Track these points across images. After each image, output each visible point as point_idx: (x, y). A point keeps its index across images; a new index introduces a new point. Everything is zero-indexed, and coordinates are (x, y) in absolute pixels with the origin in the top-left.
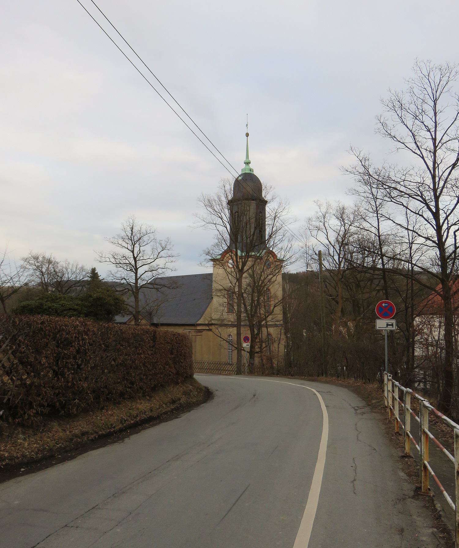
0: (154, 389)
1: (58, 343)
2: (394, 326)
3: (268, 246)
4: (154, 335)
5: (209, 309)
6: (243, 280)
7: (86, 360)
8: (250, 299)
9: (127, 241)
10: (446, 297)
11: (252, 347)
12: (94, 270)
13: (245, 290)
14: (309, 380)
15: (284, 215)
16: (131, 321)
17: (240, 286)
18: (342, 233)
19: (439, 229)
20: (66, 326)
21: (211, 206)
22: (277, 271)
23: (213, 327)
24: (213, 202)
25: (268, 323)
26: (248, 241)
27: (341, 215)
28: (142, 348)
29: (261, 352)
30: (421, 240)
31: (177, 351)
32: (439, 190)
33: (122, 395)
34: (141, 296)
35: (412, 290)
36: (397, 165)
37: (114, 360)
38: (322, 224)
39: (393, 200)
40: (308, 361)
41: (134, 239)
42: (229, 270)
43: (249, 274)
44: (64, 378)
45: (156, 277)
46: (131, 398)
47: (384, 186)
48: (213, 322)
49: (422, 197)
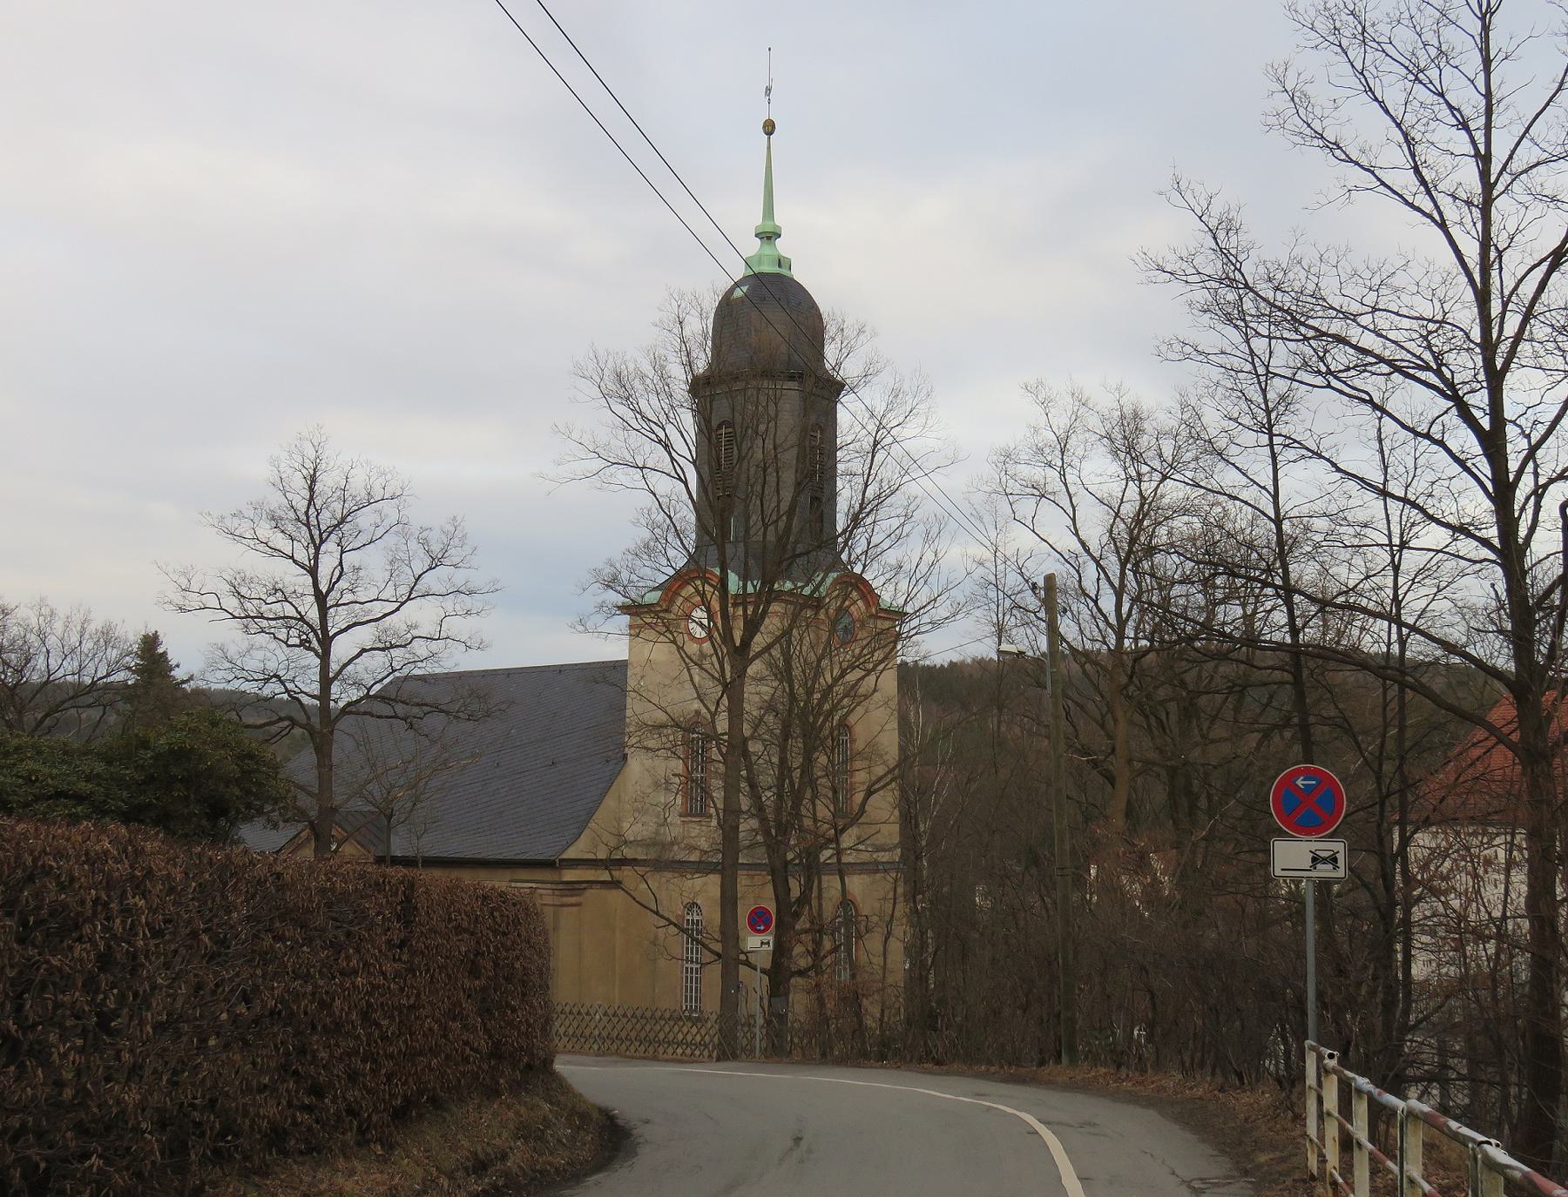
0: (401, 1115)
1: (25, 924)
2: (1341, 863)
3: (844, 557)
4: (408, 900)
5: (610, 802)
6: (749, 689)
7: (136, 995)
8: (775, 760)
9: (290, 528)
10: (1534, 753)
11: (781, 950)
12: (150, 643)
13: (755, 728)
14: (1007, 1080)
15: (915, 438)
16: (300, 847)
17: (736, 713)
18: (1129, 510)
19: (1502, 492)
20: (59, 854)
21: (627, 399)
22: (878, 655)
23: (626, 874)
24: (637, 383)
25: (845, 859)
26: (771, 537)
27: (1127, 441)
28: (358, 951)
29: (816, 967)
30: (1435, 536)
31: (496, 965)
32: (1504, 348)
33: (276, 1137)
34: (342, 746)
35: (1402, 729)
36: (1348, 250)
37: (246, 999)
38: (1053, 474)
39: (1334, 383)
40: (994, 1004)
41: (318, 523)
42: (692, 648)
43: (771, 665)
44: (46, 1064)
45: (405, 671)
46: (313, 1150)
47: (1302, 329)
48: (628, 853)
49: (1439, 373)
